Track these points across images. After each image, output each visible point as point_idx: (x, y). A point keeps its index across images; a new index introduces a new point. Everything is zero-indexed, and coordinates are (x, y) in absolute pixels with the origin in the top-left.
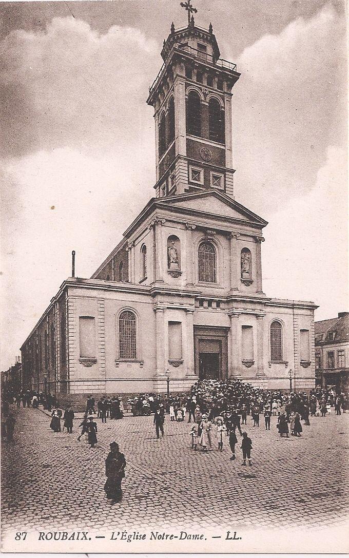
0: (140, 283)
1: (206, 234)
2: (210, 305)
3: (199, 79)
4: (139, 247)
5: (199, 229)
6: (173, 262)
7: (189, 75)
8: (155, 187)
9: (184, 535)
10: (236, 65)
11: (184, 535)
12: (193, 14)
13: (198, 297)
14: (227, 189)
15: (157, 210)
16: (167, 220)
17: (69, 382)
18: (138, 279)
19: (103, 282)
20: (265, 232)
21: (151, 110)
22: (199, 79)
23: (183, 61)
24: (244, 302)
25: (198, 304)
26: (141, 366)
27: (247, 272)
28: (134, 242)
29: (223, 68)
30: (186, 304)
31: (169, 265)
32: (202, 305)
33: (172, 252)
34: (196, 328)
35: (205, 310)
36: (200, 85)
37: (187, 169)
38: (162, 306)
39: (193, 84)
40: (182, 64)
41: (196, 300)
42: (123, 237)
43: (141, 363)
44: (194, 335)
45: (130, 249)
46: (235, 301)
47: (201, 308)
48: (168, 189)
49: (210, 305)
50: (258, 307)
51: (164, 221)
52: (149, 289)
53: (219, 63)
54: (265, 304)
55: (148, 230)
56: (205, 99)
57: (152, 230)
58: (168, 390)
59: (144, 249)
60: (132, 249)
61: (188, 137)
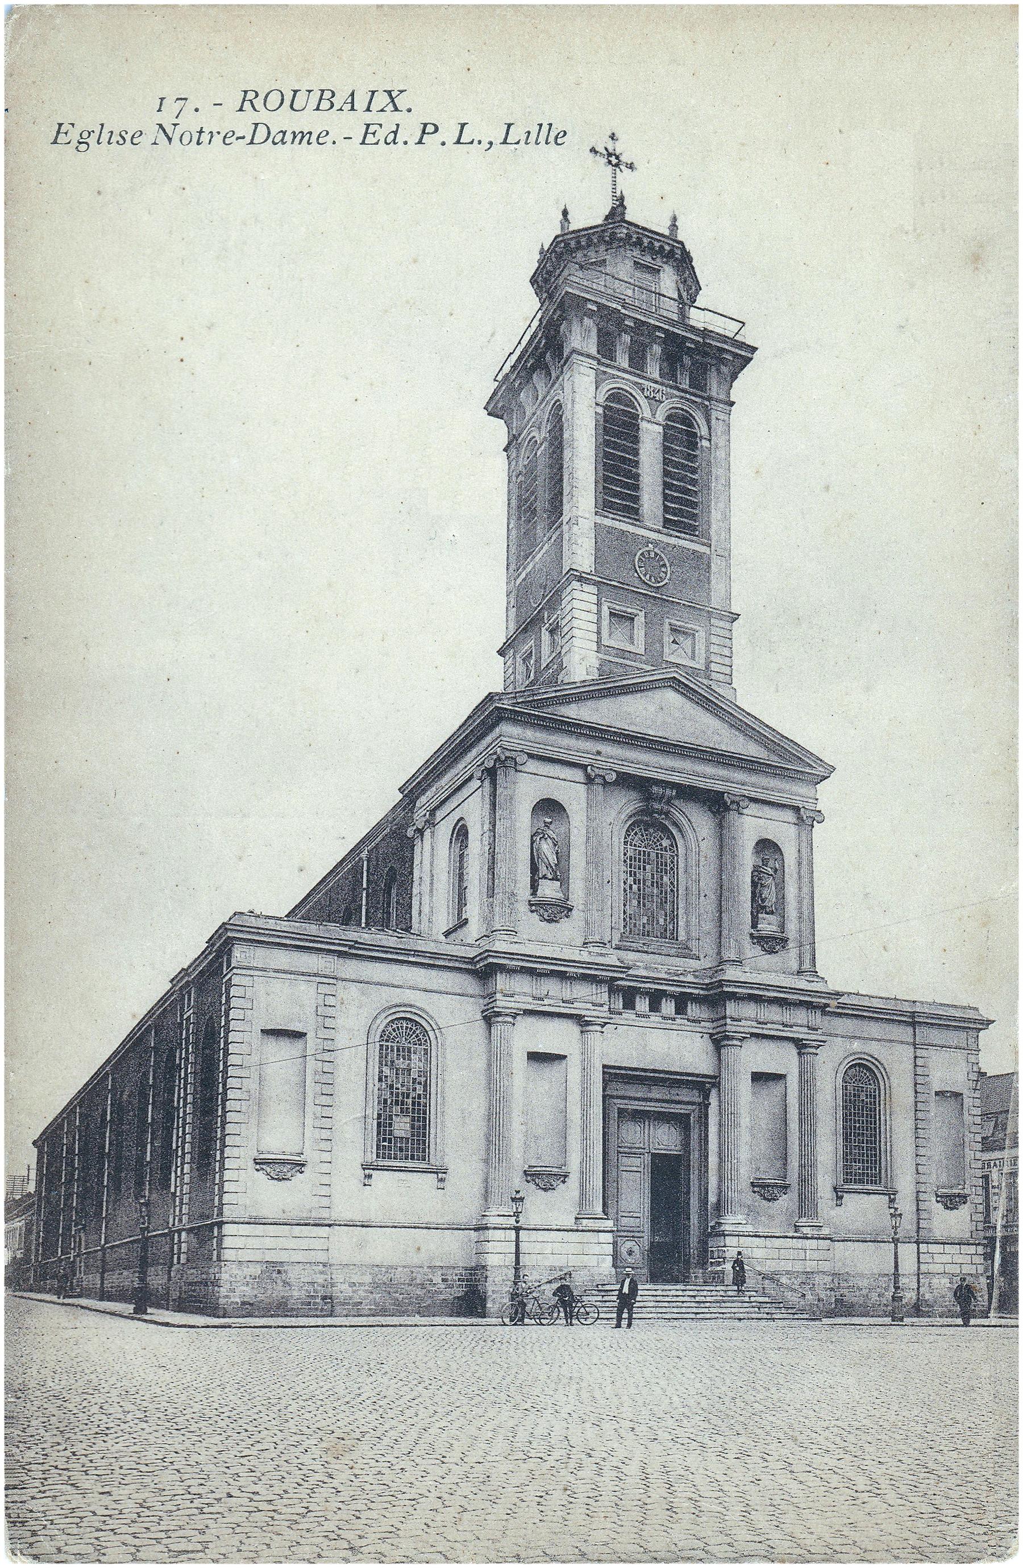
0: (447, 934)
1: (648, 797)
2: (654, 1007)
3: (638, 361)
4: (445, 830)
5: (626, 781)
6: (545, 877)
7: (606, 349)
8: (501, 652)
9: (262, 132)
10: (744, 323)
11: (262, 132)
12: (624, 176)
13: (619, 982)
14: (713, 667)
15: (506, 729)
16: (531, 756)
17: (220, 1224)
18: (443, 921)
19: (334, 930)
20: (826, 796)
21: (498, 430)
22: (638, 361)
23: (591, 314)
24: (782, 1003)
25: (619, 1004)
26: (441, 1185)
27: (772, 913)
28: (433, 812)
29: (705, 333)
30: (525, 994)
31: (534, 887)
32: (629, 1005)
33: (546, 848)
34: (613, 1075)
35: (643, 1022)
36: (639, 376)
37: (594, 608)
38: (512, 1005)
39: (620, 374)
40: (587, 321)
41: (613, 990)
42: (401, 796)
43: (440, 1172)
44: (604, 1097)
45: (420, 832)
46: (733, 996)
47: (629, 1015)
48: (538, 660)
49: (654, 1007)
50: (801, 1016)
51: (522, 758)
52: (471, 953)
53: (697, 318)
54: (823, 1009)
55: (475, 783)
56: (654, 415)
57: (487, 783)
58: (517, 1237)
59: (461, 833)
60: (427, 833)
61: (599, 520)
